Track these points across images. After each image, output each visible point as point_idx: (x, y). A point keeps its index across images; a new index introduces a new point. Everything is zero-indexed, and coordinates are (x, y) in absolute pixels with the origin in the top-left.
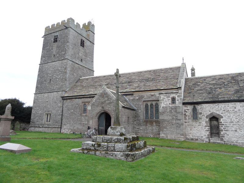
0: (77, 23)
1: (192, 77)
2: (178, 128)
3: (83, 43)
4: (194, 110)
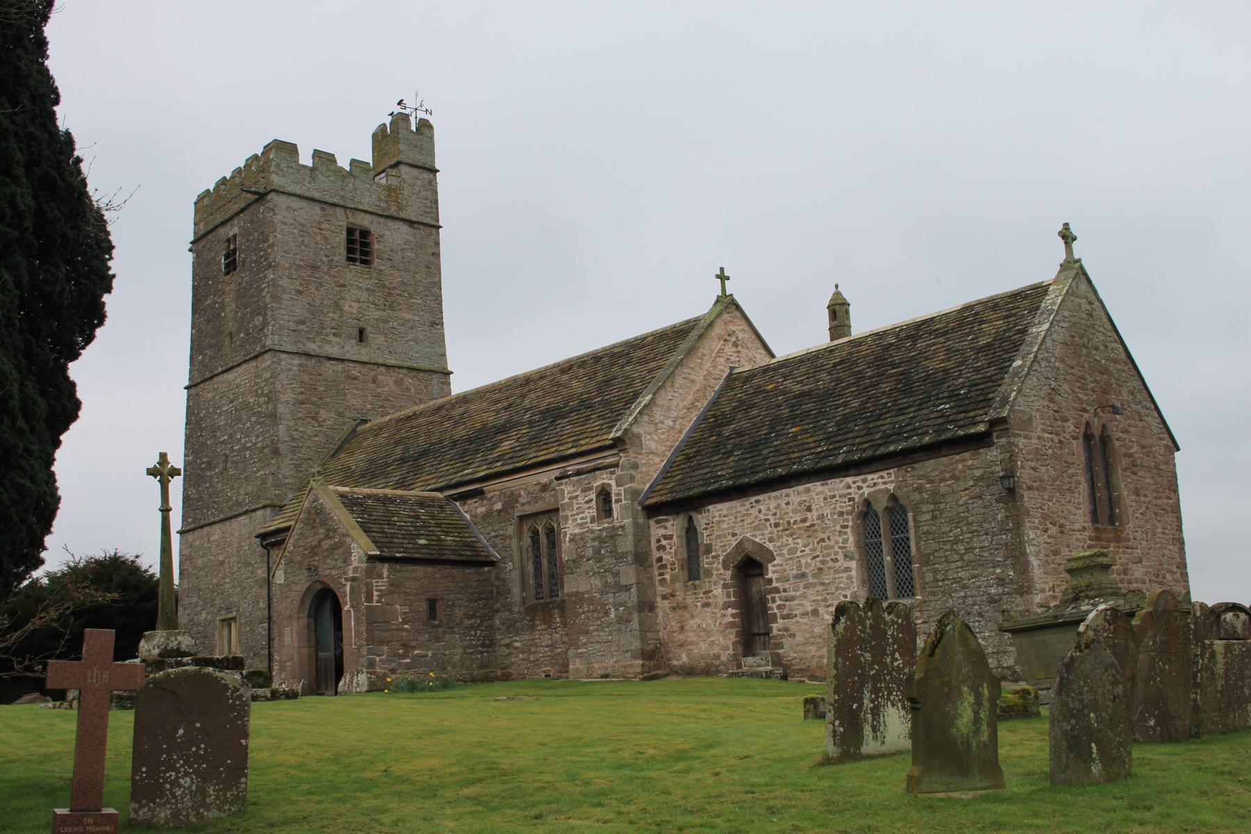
0: (317, 154)
1: (836, 342)
2: (623, 627)
3: (367, 245)
4: (691, 532)
